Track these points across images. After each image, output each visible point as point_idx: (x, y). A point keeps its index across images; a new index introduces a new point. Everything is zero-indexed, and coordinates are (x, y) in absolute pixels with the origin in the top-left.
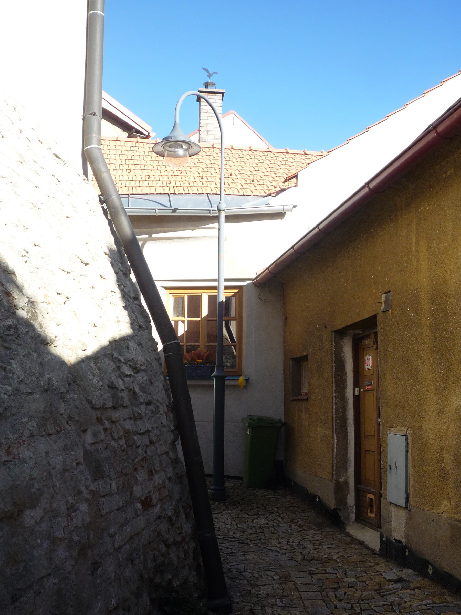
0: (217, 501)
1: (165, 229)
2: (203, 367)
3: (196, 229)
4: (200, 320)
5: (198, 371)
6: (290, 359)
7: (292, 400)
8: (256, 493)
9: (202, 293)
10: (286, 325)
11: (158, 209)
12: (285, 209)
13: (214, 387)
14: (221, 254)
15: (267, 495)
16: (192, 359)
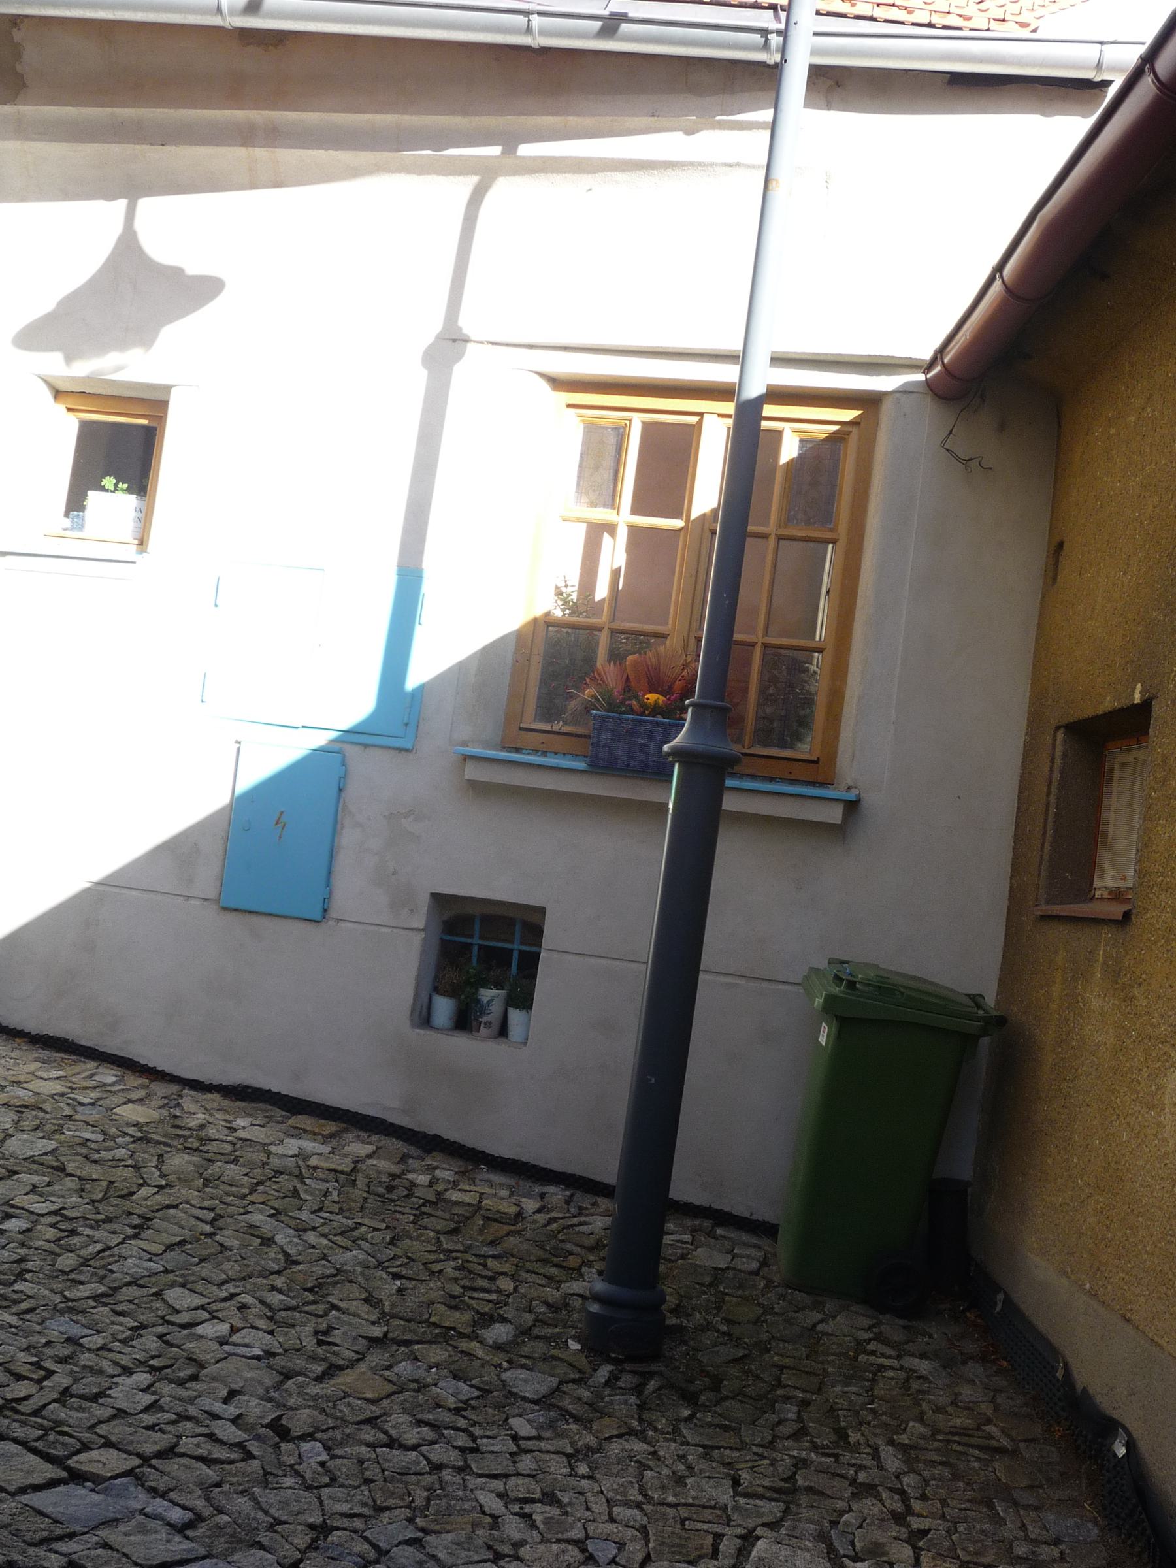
0: (611, 1361)
1: (573, 120)
2: (664, 724)
3: (702, 130)
4: (681, 529)
5: (639, 741)
6: (1058, 728)
7: (1044, 917)
8: (819, 1328)
9: (701, 414)
10: (1055, 579)
11: (540, 14)
12: (1106, 61)
13: (671, 806)
14: (775, 174)
15: (871, 1347)
16: (627, 687)
